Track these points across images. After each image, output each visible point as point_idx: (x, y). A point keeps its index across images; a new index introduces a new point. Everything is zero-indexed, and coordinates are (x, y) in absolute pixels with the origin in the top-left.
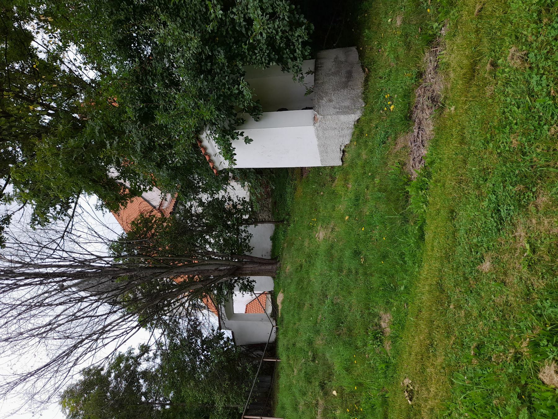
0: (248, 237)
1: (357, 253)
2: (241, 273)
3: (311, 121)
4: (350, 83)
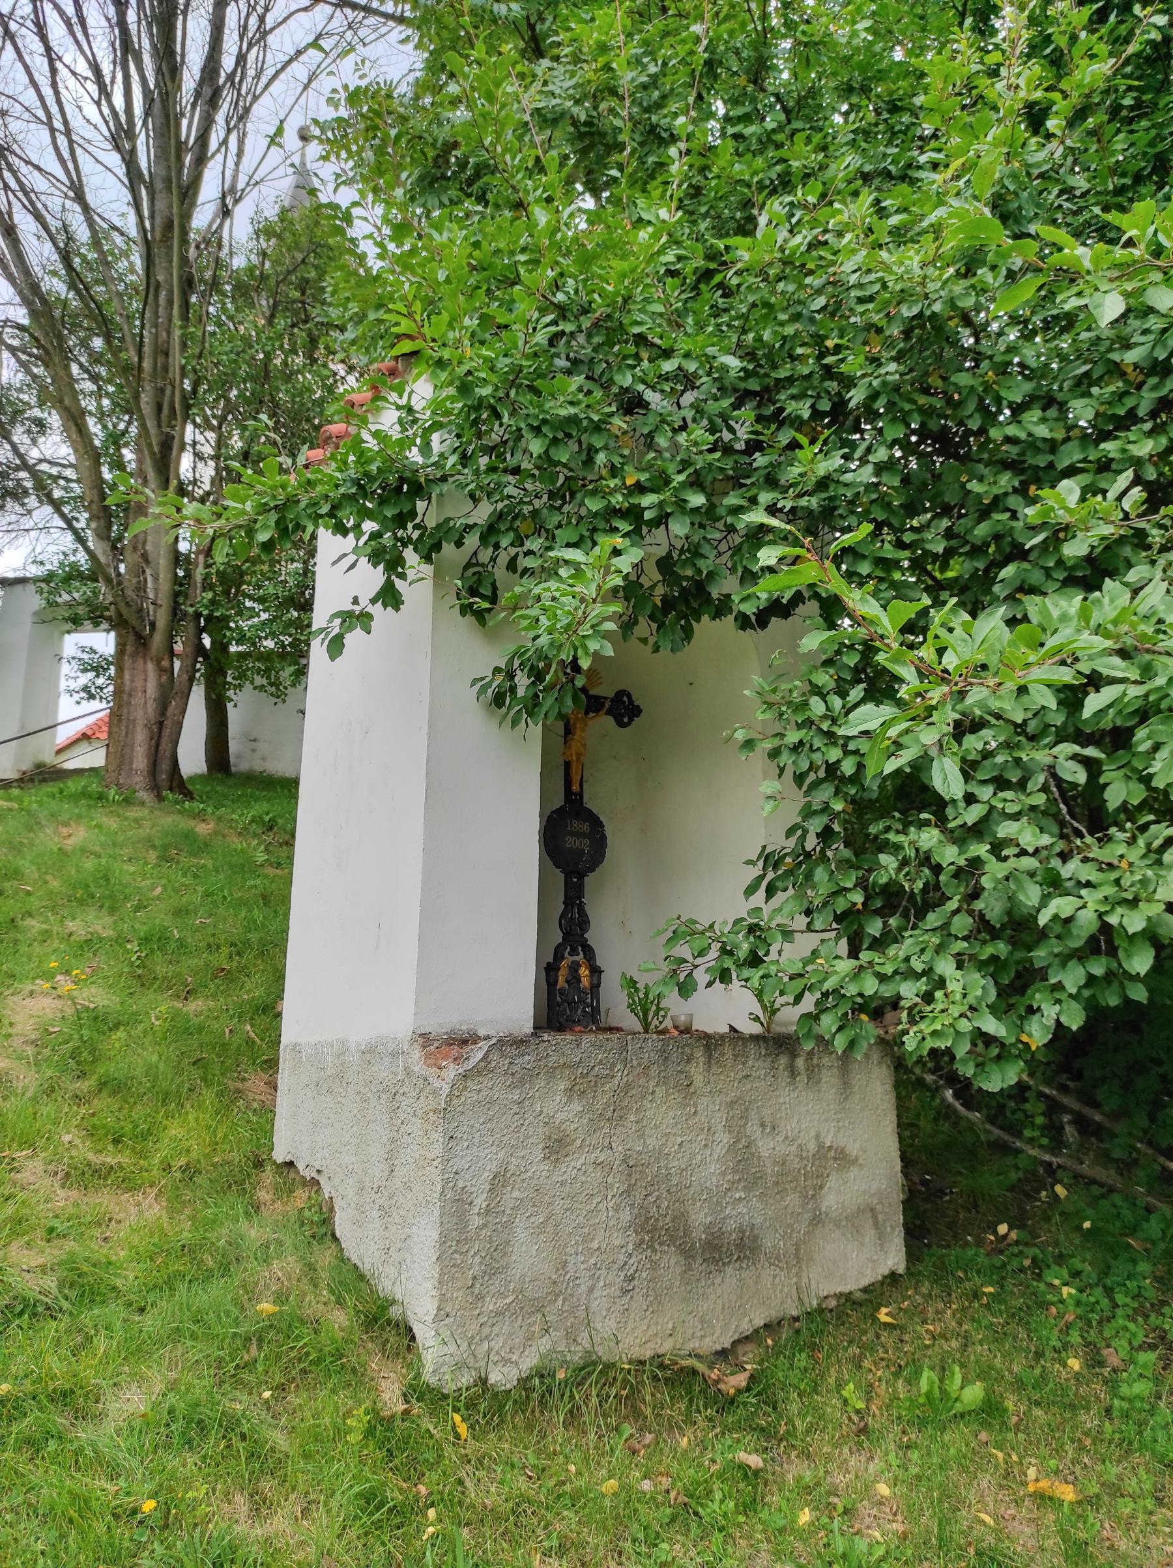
4: (671, 1260)
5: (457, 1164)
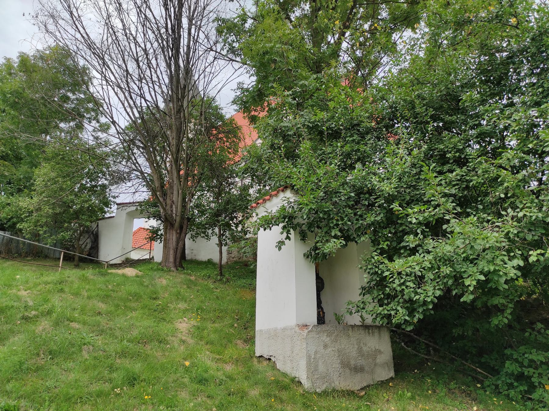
0: (207, 236)
1: (132, 380)
2: (167, 228)
3: (300, 323)
4: (348, 371)
5: (309, 349)
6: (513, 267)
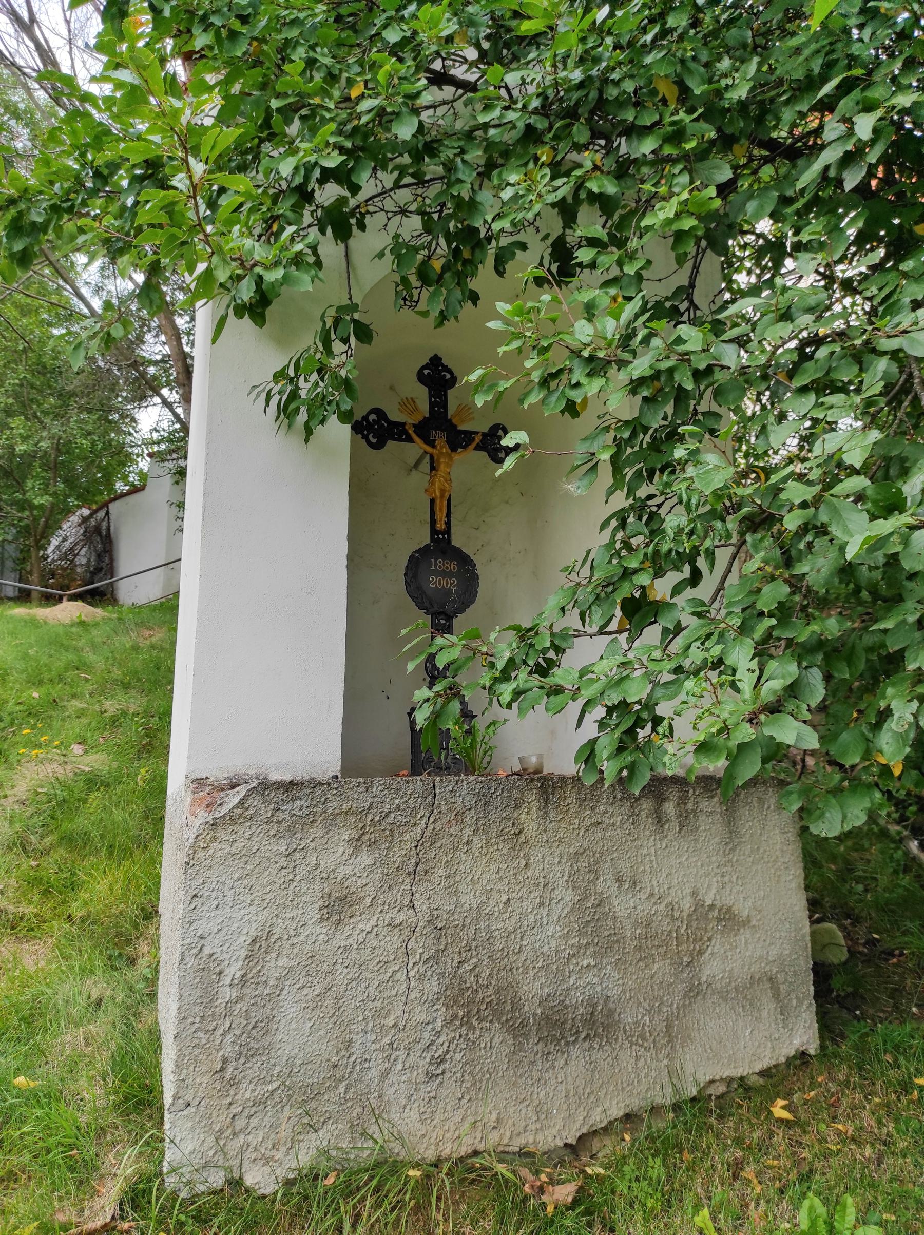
5: (203, 927)
6: (539, 282)
